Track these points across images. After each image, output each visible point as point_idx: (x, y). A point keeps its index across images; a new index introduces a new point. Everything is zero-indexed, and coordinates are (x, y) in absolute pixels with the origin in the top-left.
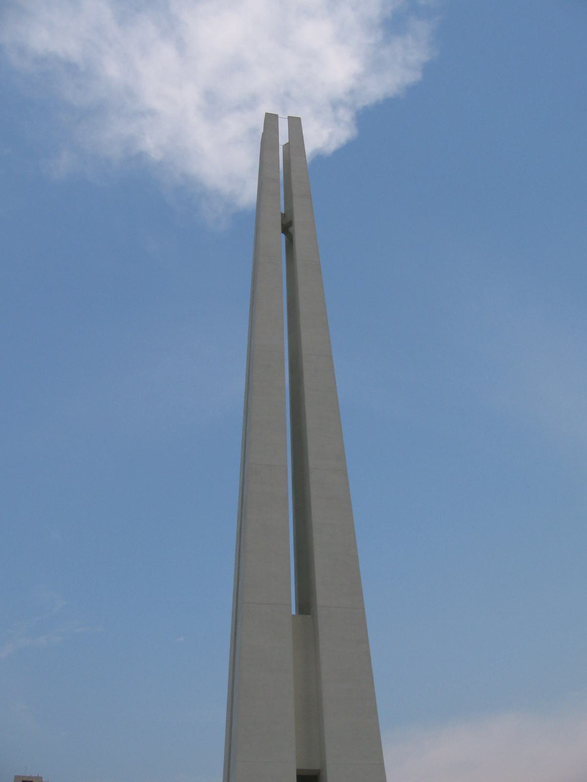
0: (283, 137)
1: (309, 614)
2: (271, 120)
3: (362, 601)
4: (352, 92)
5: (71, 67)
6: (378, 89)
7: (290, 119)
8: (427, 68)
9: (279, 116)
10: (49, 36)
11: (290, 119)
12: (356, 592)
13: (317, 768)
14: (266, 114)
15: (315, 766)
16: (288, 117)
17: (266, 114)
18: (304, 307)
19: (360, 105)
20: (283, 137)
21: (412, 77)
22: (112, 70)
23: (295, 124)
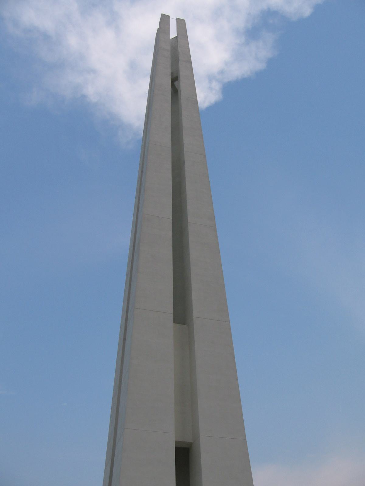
0: (173, 34)
1: (184, 324)
2: (165, 20)
3: (228, 316)
4: (222, 72)
5: (46, 37)
6: (239, 71)
7: (178, 20)
8: (270, 62)
9: (171, 17)
10: (34, 16)
11: (178, 20)
12: (224, 310)
13: (191, 441)
14: (162, 14)
15: (188, 439)
16: (177, 18)
17: (162, 14)
18: (195, 253)
19: (226, 80)
20: (173, 34)
21: (260, 66)
22: (72, 41)
23: (181, 23)
